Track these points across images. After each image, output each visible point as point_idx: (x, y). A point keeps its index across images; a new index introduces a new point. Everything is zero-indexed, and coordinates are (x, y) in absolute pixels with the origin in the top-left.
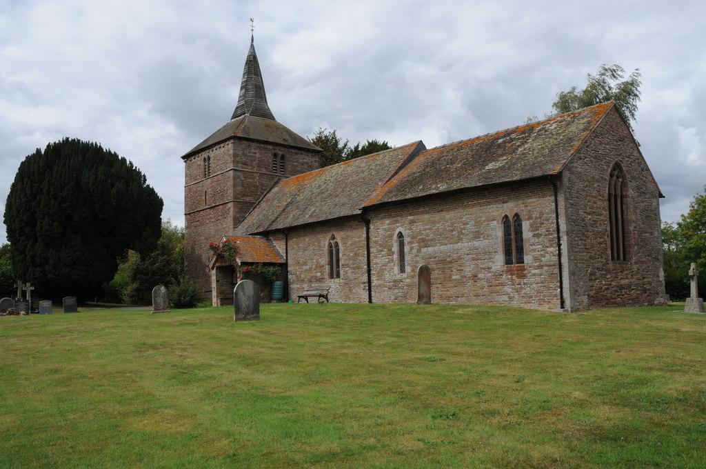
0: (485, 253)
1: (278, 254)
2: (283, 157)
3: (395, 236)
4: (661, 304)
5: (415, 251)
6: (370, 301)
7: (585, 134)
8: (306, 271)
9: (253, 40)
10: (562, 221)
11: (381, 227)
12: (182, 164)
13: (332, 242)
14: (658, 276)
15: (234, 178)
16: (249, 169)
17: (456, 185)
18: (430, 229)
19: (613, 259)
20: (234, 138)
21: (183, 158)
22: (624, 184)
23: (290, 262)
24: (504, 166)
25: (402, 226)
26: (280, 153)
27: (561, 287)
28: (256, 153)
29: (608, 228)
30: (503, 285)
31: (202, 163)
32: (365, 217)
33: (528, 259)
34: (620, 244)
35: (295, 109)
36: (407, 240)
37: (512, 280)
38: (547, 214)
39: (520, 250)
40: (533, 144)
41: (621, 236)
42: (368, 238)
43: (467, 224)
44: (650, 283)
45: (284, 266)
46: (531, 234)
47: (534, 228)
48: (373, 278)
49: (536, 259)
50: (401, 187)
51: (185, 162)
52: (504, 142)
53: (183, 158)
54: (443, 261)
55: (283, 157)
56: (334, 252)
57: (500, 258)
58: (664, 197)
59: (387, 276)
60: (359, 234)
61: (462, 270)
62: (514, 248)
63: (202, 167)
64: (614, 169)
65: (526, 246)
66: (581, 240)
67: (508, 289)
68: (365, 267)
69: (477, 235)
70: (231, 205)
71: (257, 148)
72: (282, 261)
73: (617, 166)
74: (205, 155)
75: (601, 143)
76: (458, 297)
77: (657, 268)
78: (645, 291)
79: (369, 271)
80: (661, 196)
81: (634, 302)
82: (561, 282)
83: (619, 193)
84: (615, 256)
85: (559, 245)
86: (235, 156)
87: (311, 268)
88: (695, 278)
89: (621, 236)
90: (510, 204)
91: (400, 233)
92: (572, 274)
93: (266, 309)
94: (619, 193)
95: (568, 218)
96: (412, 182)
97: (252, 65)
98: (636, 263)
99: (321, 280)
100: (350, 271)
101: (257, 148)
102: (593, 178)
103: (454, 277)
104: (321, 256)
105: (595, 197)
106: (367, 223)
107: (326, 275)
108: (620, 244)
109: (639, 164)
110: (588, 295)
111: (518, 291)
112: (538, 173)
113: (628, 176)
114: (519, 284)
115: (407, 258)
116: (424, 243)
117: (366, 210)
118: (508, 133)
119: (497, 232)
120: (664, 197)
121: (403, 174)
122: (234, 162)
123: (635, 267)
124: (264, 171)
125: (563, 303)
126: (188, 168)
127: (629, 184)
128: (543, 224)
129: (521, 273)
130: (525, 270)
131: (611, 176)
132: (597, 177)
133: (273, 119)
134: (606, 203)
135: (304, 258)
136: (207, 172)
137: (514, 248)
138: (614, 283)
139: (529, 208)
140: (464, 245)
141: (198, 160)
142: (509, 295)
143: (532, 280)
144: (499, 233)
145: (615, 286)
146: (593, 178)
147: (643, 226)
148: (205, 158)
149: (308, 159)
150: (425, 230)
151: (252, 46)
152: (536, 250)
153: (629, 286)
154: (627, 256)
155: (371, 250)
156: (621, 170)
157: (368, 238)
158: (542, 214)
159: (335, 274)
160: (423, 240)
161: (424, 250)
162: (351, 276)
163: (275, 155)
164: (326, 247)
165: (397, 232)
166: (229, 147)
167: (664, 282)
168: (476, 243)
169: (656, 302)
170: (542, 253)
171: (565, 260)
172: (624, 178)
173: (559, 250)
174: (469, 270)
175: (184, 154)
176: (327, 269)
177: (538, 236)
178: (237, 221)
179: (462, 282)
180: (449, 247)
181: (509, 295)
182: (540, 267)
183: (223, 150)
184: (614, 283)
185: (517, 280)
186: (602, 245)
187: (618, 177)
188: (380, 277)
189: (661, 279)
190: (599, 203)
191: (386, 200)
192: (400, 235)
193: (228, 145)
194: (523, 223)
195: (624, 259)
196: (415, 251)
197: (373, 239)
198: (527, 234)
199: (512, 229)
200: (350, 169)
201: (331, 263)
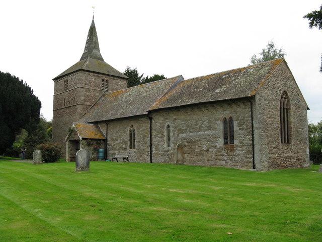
2: (107, 81)
3: (166, 128)
5: (176, 135)
6: (151, 162)
9: (93, 18)
11: (158, 121)
12: (53, 84)
16: (89, 87)
17: (199, 101)
21: (54, 80)
22: (288, 102)
23: (109, 139)
25: (169, 121)
29: (280, 126)
31: (64, 83)
32: (150, 115)
33: (236, 142)
35: (117, 57)
36: (172, 129)
37: (228, 153)
39: (232, 138)
42: (151, 127)
43: (204, 121)
45: (105, 141)
47: (240, 125)
49: (241, 142)
53: (54, 80)
54: (191, 141)
59: (161, 148)
60: (146, 125)
62: (229, 136)
65: (236, 135)
69: (209, 128)
72: (105, 138)
73: (285, 93)
74: (65, 78)
78: (299, 160)
79: (151, 145)
80: (308, 109)
84: (283, 140)
90: (227, 112)
96: (171, 99)
97: (92, 31)
98: (294, 145)
101: (90, 73)
106: (151, 119)
108: (286, 136)
111: (231, 159)
112: (242, 96)
116: (181, 131)
117: (150, 112)
124: (97, 88)
130: (234, 147)
131: (282, 98)
134: (279, 113)
136: (66, 88)
137: (229, 136)
138: (282, 156)
140: (202, 133)
141: (62, 81)
144: (221, 127)
145: (283, 157)
151: (93, 21)
153: (290, 158)
156: (287, 95)
157: (151, 127)
158: (244, 118)
159: (132, 146)
160: (180, 130)
161: (181, 135)
162: (141, 148)
163: (103, 80)
168: (209, 132)
172: (288, 99)
173: (253, 137)
174: (204, 147)
175: (53, 78)
177: (242, 129)
182: (242, 146)
184: (282, 156)
185: (230, 153)
187: (285, 99)
188: (157, 149)
191: (161, 107)
192: (168, 126)
194: (234, 122)
195: (288, 143)
198: (236, 128)
201: (130, 140)
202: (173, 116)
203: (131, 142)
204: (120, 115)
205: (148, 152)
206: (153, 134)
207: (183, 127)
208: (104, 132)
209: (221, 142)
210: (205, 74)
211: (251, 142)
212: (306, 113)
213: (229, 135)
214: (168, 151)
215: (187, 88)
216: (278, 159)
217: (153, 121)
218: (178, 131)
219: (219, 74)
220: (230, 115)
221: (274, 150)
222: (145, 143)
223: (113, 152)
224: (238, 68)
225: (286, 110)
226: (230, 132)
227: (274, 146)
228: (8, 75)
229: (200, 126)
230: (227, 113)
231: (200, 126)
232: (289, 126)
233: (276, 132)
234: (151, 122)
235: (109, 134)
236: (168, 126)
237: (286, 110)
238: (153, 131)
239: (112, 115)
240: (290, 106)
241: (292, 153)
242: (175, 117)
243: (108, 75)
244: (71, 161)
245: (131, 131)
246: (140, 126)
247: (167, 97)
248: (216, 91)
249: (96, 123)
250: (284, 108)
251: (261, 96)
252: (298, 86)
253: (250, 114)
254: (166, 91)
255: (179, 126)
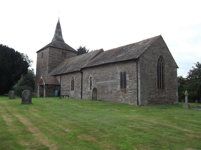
1: (58, 82)
2: (65, 53)
4: (176, 104)
5: (94, 83)
6: (82, 98)
7: (149, 45)
8: (65, 87)
10: (139, 74)
11: (86, 74)
12: (36, 54)
14: (176, 95)
15: (49, 59)
16: (54, 56)
17: (107, 62)
18: (99, 76)
19: (158, 88)
21: (37, 52)
23: (61, 85)
26: (65, 52)
27: (138, 97)
28: (56, 51)
29: (157, 78)
30: (120, 95)
31: (41, 54)
32: (81, 71)
33: (127, 87)
35: (73, 41)
36: (92, 79)
37: (122, 94)
39: (125, 84)
40: (133, 49)
41: (162, 80)
43: (110, 74)
44: (172, 97)
45: (60, 86)
47: (130, 77)
48: (83, 91)
49: (130, 87)
50: (92, 63)
53: (37, 52)
54: (102, 87)
55: (65, 53)
57: (119, 86)
59: (87, 91)
62: (123, 83)
65: (127, 83)
66: (146, 81)
67: (121, 97)
69: (113, 78)
70: (48, 67)
71: (58, 50)
72: (59, 84)
73: (161, 57)
74: (42, 52)
75: (155, 49)
78: (170, 99)
80: (178, 68)
81: (167, 103)
82: (138, 95)
83: (161, 66)
84: (159, 87)
85: (138, 82)
86: (50, 52)
87: (66, 87)
89: (162, 80)
90: (123, 68)
92: (141, 93)
93: (33, 100)
95: (141, 73)
97: (58, 26)
99: (69, 91)
101: (58, 50)
102: (152, 60)
103: (105, 92)
105: (152, 67)
106: (82, 73)
107: (70, 89)
108: (161, 83)
110: (148, 100)
111: (124, 97)
112: (131, 58)
113: (165, 60)
115: (92, 85)
116: (97, 80)
117: (82, 69)
121: (96, 58)
123: (167, 91)
124: (59, 57)
125: (138, 102)
127: (166, 63)
128: (133, 75)
129: (125, 92)
131: (159, 60)
132: (153, 60)
133: (64, 42)
134: (156, 69)
135: (65, 83)
136: (42, 57)
137: (123, 83)
138: (158, 96)
139: (129, 70)
141: (40, 53)
142: (121, 99)
143: (129, 94)
144: (119, 78)
145: (159, 97)
146: (152, 60)
149: (73, 54)
151: (59, 21)
152: (131, 84)
153: (164, 98)
154: (164, 87)
155: (83, 82)
156: (163, 58)
157: (82, 78)
160: (97, 79)
161: (97, 83)
163: (63, 52)
166: (48, 49)
168: (112, 81)
169: (174, 103)
171: (139, 88)
173: (138, 84)
174: (110, 90)
178: (49, 72)
179: (107, 94)
180: (105, 82)
181: (121, 99)
182: (131, 90)
184: (158, 96)
187: (161, 61)
188: (85, 90)
190: (154, 69)
191: (87, 66)
192: (91, 78)
195: (163, 88)
196: (94, 83)
198: (128, 79)
199: (123, 76)
200: (82, 57)
201: (72, 86)
202: (93, 71)
206: (83, 82)
208: (59, 81)
210: (115, 48)
211: (136, 87)
212: (177, 70)
213: (123, 83)
216: (155, 98)
219: (123, 47)
220: (124, 71)
222: (79, 87)
225: (161, 68)
226: (124, 81)
227: (153, 90)
228: (12, 50)
230: (119, 69)
232: (164, 77)
233: (154, 81)
234: (82, 75)
235: (62, 82)
236: (91, 78)
237: (161, 68)
238: (83, 80)
239: (64, 72)
241: (166, 95)
242: (94, 72)
243: (66, 50)
244: (40, 97)
247: (92, 61)
249: (55, 76)
252: (170, 53)
253: (136, 70)
254: (92, 57)
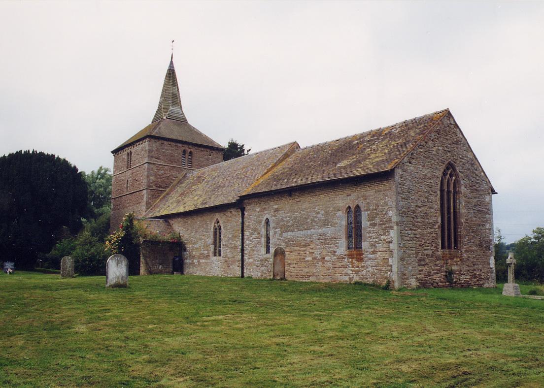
0: (331, 239)
2: (191, 153)
3: (263, 222)
5: (277, 235)
9: (172, 57)
11: (253, 212)
12: (112, 157)
13: (216, 225)
17: (310, 180)
20: (150, 137)
21: (112, 152)
22: (456, 183)
24: (351, 164)
25: (269, 214)
26: (189, 150)
28: (168, 149)
29: (439, 220)
31: (126, 158)
32: (240, 204)
33: (365, 245)
34: (450, 234)
36: (272, 225)
37: (352, 263)
38: (381, 206)
42: (243, 223)
43: (318, 213)
46: (368, 223)
47: (371, 218)
48: (246, 257)
49: (373, 245)
51: (114, 156)
52: (358, 143)
53: (112, 152)
56: (218, 233)
58: (497, 193)
60: (234, 217)
61: (313, 253)
62: (355, 234)
63: (126, 160)
64: (448, 168)
66: (411, 229)
68: (240, 247)
69: (326, 223)
71: (171, 143)
73: (450, 166)
74: (128, 150)
76: (310, 276)
77: (488, 257)
78: (475, 276)
79: (242, 250)
80: (493, 192)
83: (452, 189)
86: (150, 151)
88: (513, 266)
90: (354, 195)
91: (267, 219)
94: (452, 189)
96: (276, 179)
97: (171, 75)
98: (467, 251)
100: (229, 250)
101: (171, 143)
104: (209, 237)
106: (243, 210)
107: (211, 254)
108: (450, 234)
109: (472, 165)
110: (417, 278)
114: (358, 267)
116: (286, 228)
118: (362, 136)
119: (342, 221)
120: (497, 193)
122: (149, 156)
126: (116, 161)
127: (462, 182)
130: (363, 254)
131: (444, 174)
132: (429, 175)
135: (196, 237)
137: (355, 234)
140: (315, 232)
141: (124, 155)
143: (369, 263)
147: (474, 219)
148: (128, 154)
150: (286, 217)
151: (172, 63)
156: (454, 170)
157: (243, 223)
158: (377, 206)
159: (217, 252)
162: (230, 255)
164: (212, 230)
165: (265, 219)
166: (146, 144)
167: (494, 270)
170: (377, 240)
172: (457, 176)
175: (111, 151)
176: (212, 247)
177: (374, 225)
183: (141, 146)
185: (356, 263)
186: (432, 235)
187: (451, 176)
189: (491, 267)
193: (145, 142)
194: (363, 213)
195: (456, 245)
197: (246, 224)
198: (365, 223)
201: (215, 243)
202: (274, 205)
203: (215, 246)
204: (202, 204)
205: (239, 261)
206: (247, 233)
207: (288, 222)
209: (342, 248)
214: (266, 260)
215: (301, 160)
217: (246, 213)
218: (281, 228)
221: (427, 261)
223: (191, 261)
224: (378, 128)
229: (313, 221)
231: (313, 221)
233: (432, 230)
234: (243, 215)
240: (460, 187)
242: (276, 207)
245: (216, 229)
246: (228, 220)
248: (338, 165)
250: (449, 192)
251: (405, 171)
255: (282, 220)
